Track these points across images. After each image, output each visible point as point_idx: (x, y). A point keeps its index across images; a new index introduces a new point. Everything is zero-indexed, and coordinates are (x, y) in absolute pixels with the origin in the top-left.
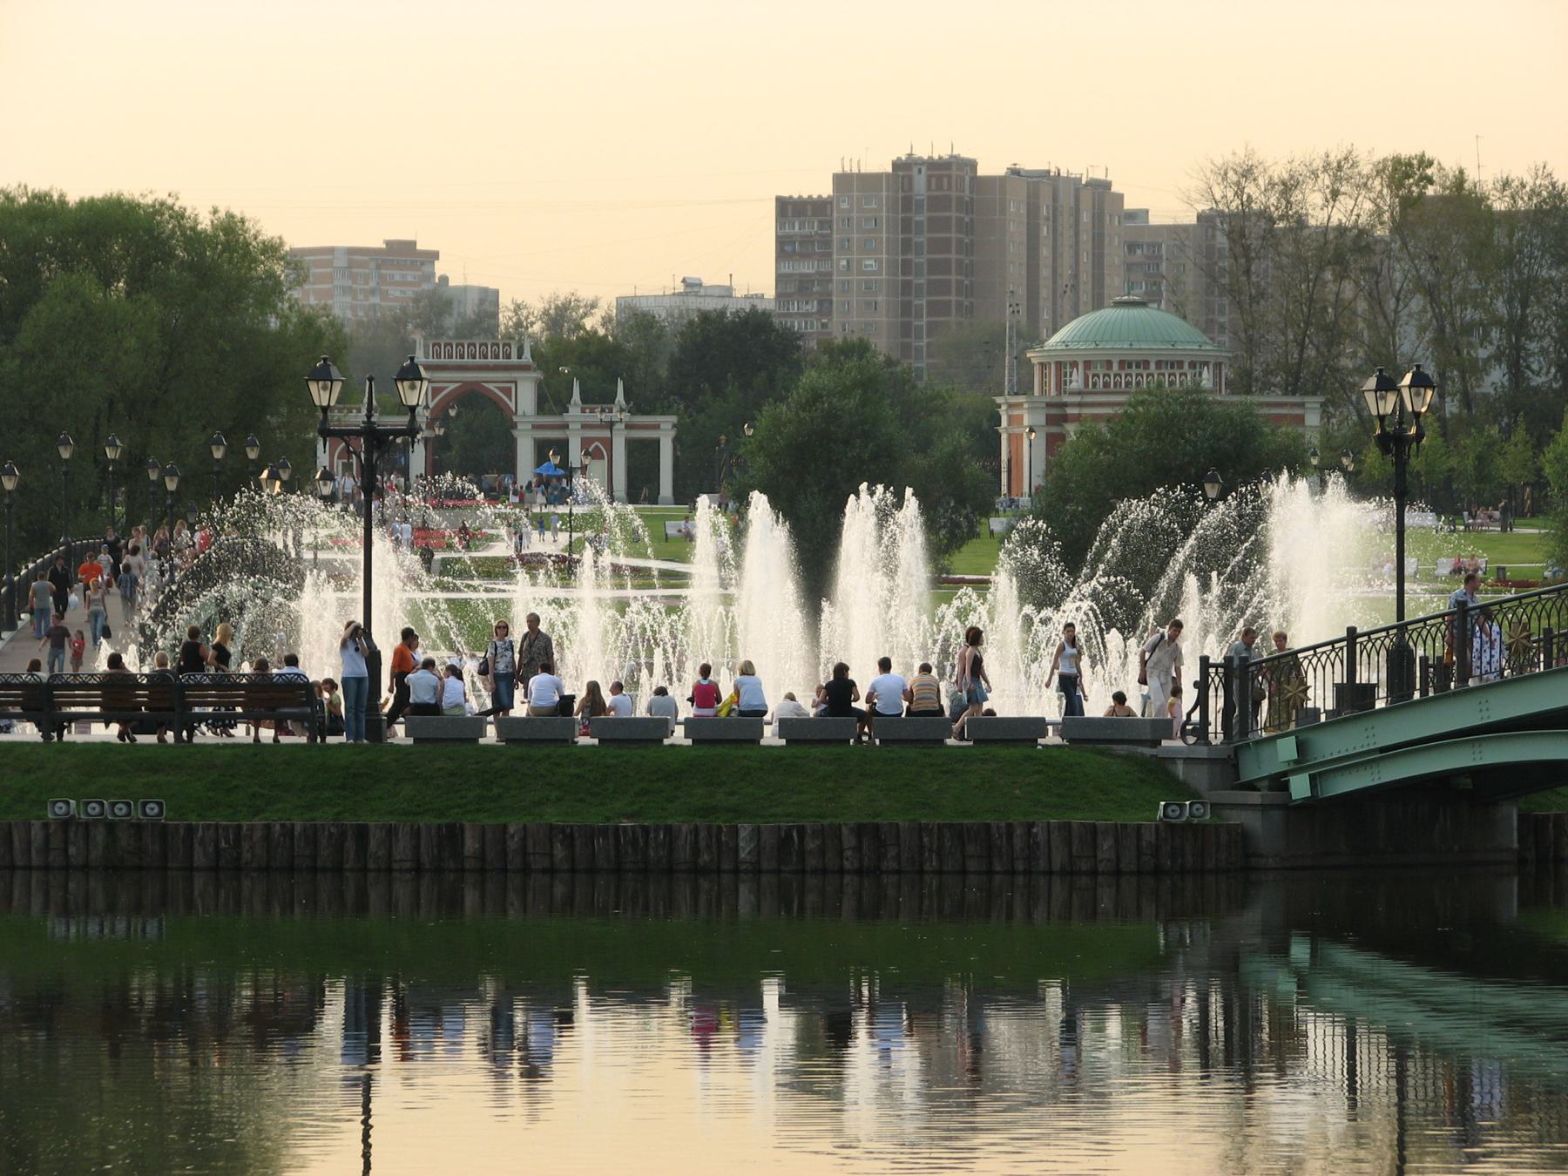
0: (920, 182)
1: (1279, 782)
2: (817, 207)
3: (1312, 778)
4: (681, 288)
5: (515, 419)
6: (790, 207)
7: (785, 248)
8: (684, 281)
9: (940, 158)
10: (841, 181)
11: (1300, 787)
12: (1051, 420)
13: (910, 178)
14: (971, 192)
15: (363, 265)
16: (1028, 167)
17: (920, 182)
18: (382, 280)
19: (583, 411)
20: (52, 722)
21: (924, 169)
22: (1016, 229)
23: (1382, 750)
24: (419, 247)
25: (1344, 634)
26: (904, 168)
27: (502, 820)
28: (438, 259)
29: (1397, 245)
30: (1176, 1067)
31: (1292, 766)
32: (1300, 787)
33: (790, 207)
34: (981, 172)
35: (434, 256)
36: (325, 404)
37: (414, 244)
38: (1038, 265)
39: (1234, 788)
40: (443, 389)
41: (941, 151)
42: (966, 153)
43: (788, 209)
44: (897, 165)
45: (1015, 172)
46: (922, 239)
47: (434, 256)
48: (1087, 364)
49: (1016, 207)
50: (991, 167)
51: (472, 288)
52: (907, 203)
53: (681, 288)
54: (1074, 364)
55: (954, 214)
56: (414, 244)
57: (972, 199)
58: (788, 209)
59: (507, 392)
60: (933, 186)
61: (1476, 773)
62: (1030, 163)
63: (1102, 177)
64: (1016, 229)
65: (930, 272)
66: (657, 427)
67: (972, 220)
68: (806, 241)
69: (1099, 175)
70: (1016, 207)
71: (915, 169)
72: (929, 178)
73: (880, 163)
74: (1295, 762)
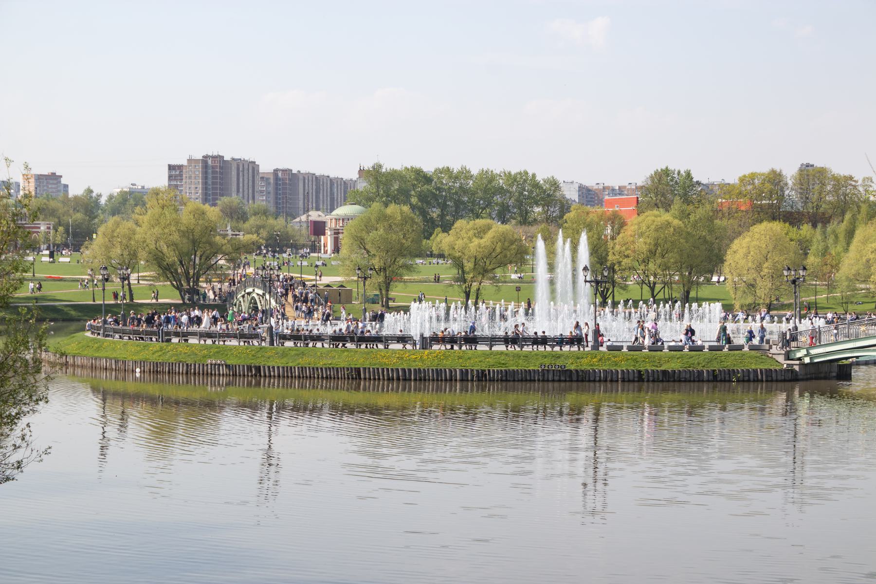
2: (180, 167)
3: (810, 358)
11: (807, 360)
12: (335, 233)
15: (42, 179)
18: (47, 183)
24: (57, 174)
26: (276, 171)
27: (124, 328)
35: (61, 176)
42: (290, 168)
43: (171, 167)
45: (233, 159)
46: (281, 187)
47: (61, 176)
48: (343, 220)
55: (218, 170)
62: (236, 157)
64: (234, 173)
65: (212, 185)
68: (176, 176)
72: (212, 161)
73: (199, 156)
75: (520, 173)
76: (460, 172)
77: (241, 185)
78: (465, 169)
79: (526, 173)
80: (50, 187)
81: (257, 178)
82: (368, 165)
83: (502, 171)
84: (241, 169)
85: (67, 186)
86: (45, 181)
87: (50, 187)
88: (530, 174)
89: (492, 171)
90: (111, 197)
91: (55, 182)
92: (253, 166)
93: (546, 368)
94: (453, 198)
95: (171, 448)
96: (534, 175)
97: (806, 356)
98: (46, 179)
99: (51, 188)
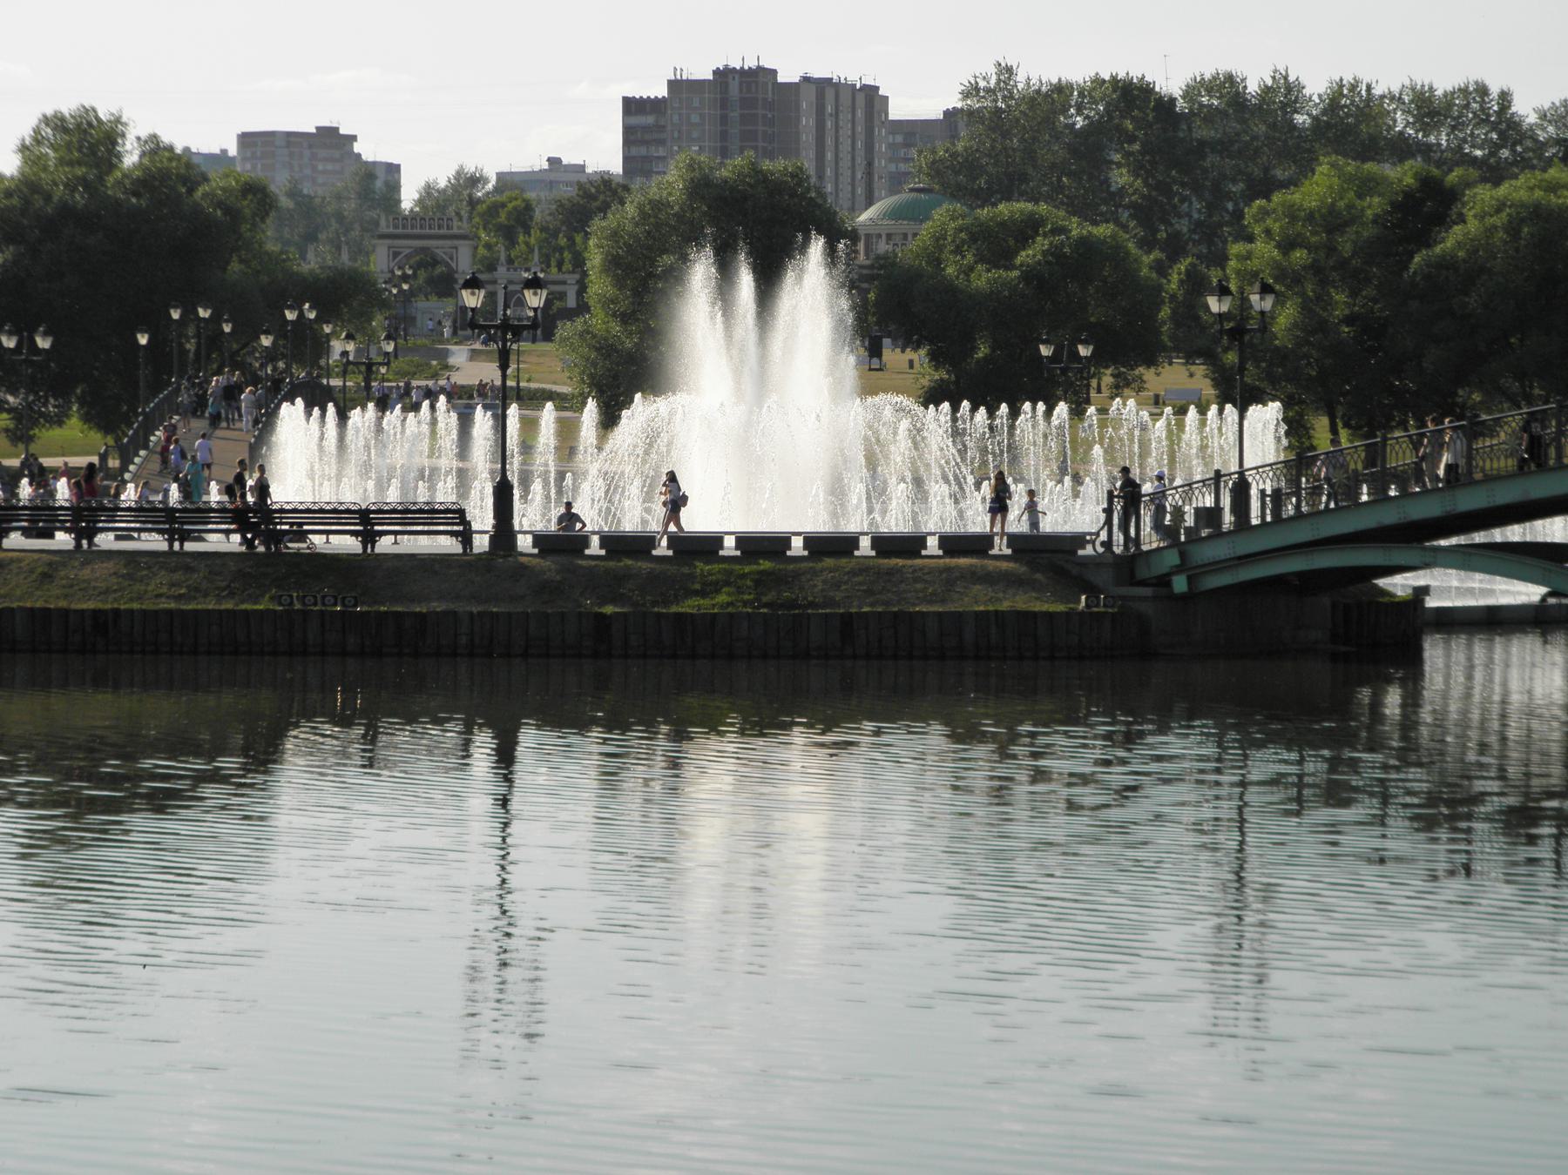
0: (734, 86)
1: (1164, 581)
3: (1190, 579)
4: (546, 166)
5: (456, 276)
6: (633, 106)
7: (631, 136)
8: (549, 160)
9: (750, 68)
10: (673, 85)
11: (1180, 584)
13: (727, 84)
14: (773, 94)
16: (816, 76)
17: (734, 86)
19: (508, 270)
20: (369, 537)
21: (737, 77)
22: (807, 121)
23: (1239, 558)
24: (342, 132)
25: (1212, 475)
26: (723, 74)
28: (356, 140)
29: (1242, 205)
30: (468, 765)
31: (1175, 569)
32: (1180, 584)
33: (633, 106)
34: (780, 79)
35: (353, 138)
36: (473, 306)
37: (337, 129)
38: (817, 146)
39: (1132, 584)
40: (399, 253)
41: (751, 63)
42: (767, 63)
43: (632, 106)
44: (716, 72)
47: (353, 138)
49: (807, 103)
50: (788, 74)
51: (381, 163)
52: (724, 103)
53: (546, 166)
54: (879, 236)
55: (760, 112)
56: (337, 129)
57: (773, 100)
58: (632, 106)
59: (451, 259)
60: (744, 90)
61: (1301, 575)
63: (873, 84)
64: (807, 121)
66: (564, 283)
67: (774, 116)
69: (868, 81)
70: (807, 103)
71: (731, 77)
72: (741, 84)
74: (1177, 566)
75: (1464, 91)
76: (1267, 90)
77: (829, 141)
78: (1286, 78)
79: (1483, 90)
80: (320, 167)
81: (880, 133)
82: (49, 112)
83: (1407, 83)
84: (829, 109)
85: (398, 167)
86: (307, 153)
87: (320, 167)
88: (1494, 91)
89: (1369, 88)
90: (428, 189)
91: (337, 154)
92: (871, 98)
93: (298, 606)
94: (1550, 159)
95: (765, 813)
96: (1505, 98)
97: (1178, 570)
98: (310, 147)
99: (324, 172)
